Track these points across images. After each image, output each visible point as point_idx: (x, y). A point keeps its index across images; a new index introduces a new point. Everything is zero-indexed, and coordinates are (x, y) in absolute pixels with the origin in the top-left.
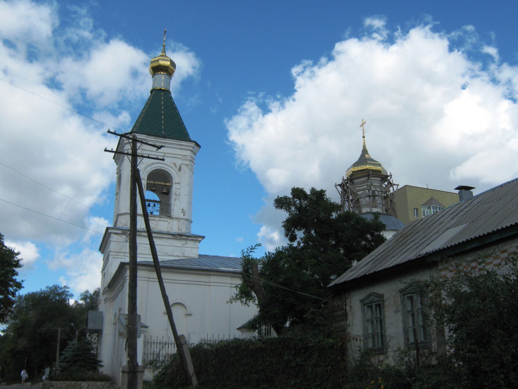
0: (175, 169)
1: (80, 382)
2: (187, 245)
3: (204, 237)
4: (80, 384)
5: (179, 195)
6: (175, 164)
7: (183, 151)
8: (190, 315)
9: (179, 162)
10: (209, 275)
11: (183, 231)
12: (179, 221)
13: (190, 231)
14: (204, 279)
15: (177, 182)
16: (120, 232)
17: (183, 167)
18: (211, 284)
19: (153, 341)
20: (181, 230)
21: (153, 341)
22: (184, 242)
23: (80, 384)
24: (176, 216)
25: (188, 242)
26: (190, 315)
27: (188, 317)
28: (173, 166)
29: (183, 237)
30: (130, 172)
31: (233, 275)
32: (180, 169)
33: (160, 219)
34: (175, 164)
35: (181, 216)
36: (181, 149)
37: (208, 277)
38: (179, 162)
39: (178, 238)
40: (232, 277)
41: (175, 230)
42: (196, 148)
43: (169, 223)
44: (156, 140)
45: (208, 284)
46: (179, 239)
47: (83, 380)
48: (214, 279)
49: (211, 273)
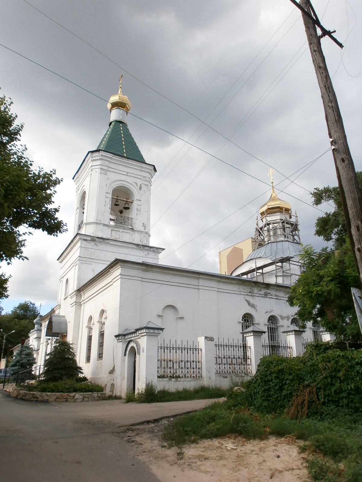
0: (136, 187)
1: (72, 394)
2: (149, 256)
3: (164, 249)
4: (74, 397)
5: (140, 211)
6: (136, 184)
7: (143, 173)
8: (182, 318)
9: (139, 182)
10: (198, 278)
11: (144, 243)
12: (141, 233)
13: (149, 244)
14: (194, 282)
15: (138, 199)
16: (89, 238)
17: (143, 186)
18: (200, 287)
19: (166, 346)
20: (142, 242)
21: (172, 346)
22: (146, 253)
23: (74, 397)
24: (138, 229)
25: (150, 253)
26: (182, 318)
27: (179, 321)
28: (135, 185)
29: (145, 248)
30: (305, 33)
31: (219, 279)
32: (141, 187)
33: (123, 231)
34: (136, 184)
35: (142, 229)
36: (142, 171)
37: (197, 280)
38: (139, 182)
39: (142, 248)
40: (219, 281)
41: (137, 242)
42: (153, 171)
43: (132, 235)
44: (120, 160)
45: (197, 287)
46: (142, 250)
47: (76, 390)
48: (203, 282)
49: (201, 276)
